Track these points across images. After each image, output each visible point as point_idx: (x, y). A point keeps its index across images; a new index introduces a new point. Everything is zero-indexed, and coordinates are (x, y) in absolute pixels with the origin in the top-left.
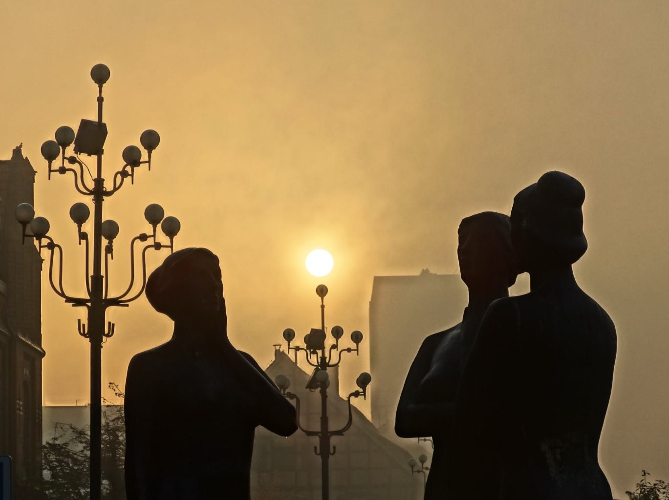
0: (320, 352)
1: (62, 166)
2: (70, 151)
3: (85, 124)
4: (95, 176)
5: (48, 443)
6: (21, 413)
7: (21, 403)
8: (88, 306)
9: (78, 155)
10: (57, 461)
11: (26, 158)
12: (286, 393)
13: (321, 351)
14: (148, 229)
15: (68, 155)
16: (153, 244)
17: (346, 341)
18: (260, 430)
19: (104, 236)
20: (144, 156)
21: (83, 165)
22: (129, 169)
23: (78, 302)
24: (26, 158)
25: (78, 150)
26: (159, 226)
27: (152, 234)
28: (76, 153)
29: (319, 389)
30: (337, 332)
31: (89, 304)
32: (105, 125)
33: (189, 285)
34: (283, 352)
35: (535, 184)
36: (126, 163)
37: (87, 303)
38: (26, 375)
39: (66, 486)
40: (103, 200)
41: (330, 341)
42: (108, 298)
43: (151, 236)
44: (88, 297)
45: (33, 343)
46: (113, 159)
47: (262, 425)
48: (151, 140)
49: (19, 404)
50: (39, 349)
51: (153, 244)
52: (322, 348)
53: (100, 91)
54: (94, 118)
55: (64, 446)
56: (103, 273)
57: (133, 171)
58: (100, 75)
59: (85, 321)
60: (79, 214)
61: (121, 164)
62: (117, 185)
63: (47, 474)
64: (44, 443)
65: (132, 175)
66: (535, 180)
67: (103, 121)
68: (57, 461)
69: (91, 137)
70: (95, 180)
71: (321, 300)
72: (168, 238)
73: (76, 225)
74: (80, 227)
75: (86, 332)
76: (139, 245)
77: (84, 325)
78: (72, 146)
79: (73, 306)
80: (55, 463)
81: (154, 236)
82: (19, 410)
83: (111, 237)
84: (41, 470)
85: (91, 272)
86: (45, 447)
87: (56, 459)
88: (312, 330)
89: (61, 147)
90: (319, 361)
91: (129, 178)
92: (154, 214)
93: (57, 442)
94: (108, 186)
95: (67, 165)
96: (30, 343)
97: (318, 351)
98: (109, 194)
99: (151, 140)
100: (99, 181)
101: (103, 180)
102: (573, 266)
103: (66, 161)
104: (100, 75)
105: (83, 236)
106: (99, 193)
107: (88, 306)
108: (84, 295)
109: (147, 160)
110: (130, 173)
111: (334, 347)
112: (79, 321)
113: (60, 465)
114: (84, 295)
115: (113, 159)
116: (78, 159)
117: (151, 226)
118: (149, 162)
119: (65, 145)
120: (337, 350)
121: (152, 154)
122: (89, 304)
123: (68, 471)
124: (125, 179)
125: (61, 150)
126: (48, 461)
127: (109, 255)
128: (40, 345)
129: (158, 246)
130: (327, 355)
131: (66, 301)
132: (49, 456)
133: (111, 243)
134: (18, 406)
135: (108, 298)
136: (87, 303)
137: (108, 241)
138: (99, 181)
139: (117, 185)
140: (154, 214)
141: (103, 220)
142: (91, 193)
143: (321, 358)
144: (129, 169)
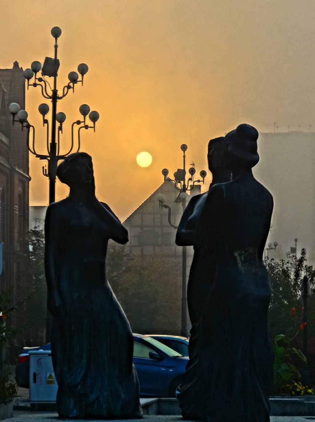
0: (182, 182)
1: (34, 82)
2: (39, 75)
3: (47, 60)
4: (53, 88)
5: (31, 230)
6: (17, 213)
7: (17, 207)
8: (48, 159)
9: (44, 76)
10: (36, 240)
11: (21, 67)
12: (163, 204)
13: (183, 181)
14: (81, 118)
15: (37, 77)
16: (84, 126)
17: (197, 176)
18: (111, 241)
19: (58, 121)
20: (80, 78)
21: (46, 82)
22: (71, 84)
23: (42, 157)
24: (21, 67)
25: (44, 74)
26: (87, 116)
27: (83, 121)
28: (43, 75)
29: (181, 203)
30: (192, 171)
31: (49, 158)
32: (58, 60)
33: (76, 170)
34: (169, 178)
35: (234, 130)
36: (70, 81)
37: (48, 158)
38: (20, 191)
39: (41, 254)
40: (57, 102)
41: (188, 176)
42: (59, 155)
43: (82, 122)
44: (48, 155)
45: (24, 173)
46: (63, 79)
47: (111, 238)
48: (83, 69)
49: (16, 208)
50: (28, 176)
51: (84, 126)
52: (184, 180)
53: (56, 42)
54: (53, 57)
55: (40, 232)
56: (57, 141)
57: (73, 85)
58: (56, 33)
59: (47, 168)
60: (43, 110)
61: (67, 81)
62: (65, 93)
63: (31, 248)
64: (30, 230)
65: (73, 88)
66: (235, 128)
67: (57, 58)
68: (36, 240)
69: (51, 67)
70: (52, 91)
71: (183, 153)
72: (92, 122)
73: (42, 115)
74: (44, 116)
75: (47, 173)
76: (76, 127)
77: (46, 170)
78: (41, 71)
79: (40, 159)
80: (35, 241)
81: (84, 122)
82: (16, 211)
83: (61, 122)
84: (28, 245)
85: (50, 141)
86: (29, 232)
87: (36, 239)
88: (179, 170)
89: (34, 73)
90: (182, 187)
91: (72, 89)
92: (84, 110)
93: (37, 230)
94: (60, 93)
95: (37, 82)
96: (22, 173)
97: (181, 181)
98: (60, 98)
99: (83, 69)
100: (55, 92)
101: (57, 91)
102: (252, 168)
103: (37, 80)
104: (56, 33)
105: (46, 121)
106: (55, 98)
107: (48, 159)
108: (46, 153)
109: (81, 80)
110: (72, 86)
111: (190, 179)
112: (43, 167)
113: (38, 242)
114: (46, 153)
115: (63, 79)
116: (43, 79)
117: (83, 116)
118: (82, 81)
119: (36, 71)
120: (192, 181)
121: (84, 77)
122: (49, 158)
123: (43, 246)
124: (69, 90)
125: (34, 74)
126: (32, 240)
127: (60, 131)
128: (28, 174)
129: (86, 127)
130: (186, 184)
131: (36, 157)
132: (32, 237)
133: (61, 125)
134: (15, 209)
135: (59, 155)
136: (48, 158)
137: (60, 124)
138: (55, 92)
139: (65, 93)
140: (84, 110)
141: (57, 112)
142: (50, 98)
143: (183, 185)
144: (71, 84)
